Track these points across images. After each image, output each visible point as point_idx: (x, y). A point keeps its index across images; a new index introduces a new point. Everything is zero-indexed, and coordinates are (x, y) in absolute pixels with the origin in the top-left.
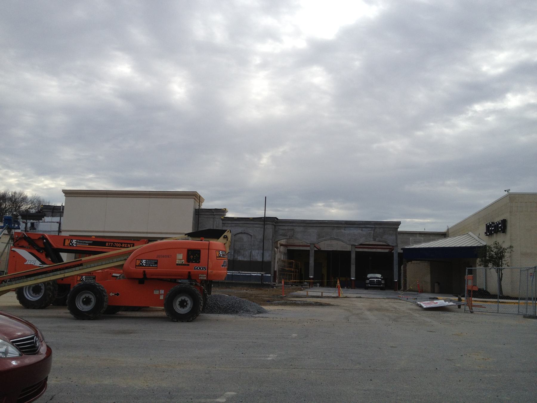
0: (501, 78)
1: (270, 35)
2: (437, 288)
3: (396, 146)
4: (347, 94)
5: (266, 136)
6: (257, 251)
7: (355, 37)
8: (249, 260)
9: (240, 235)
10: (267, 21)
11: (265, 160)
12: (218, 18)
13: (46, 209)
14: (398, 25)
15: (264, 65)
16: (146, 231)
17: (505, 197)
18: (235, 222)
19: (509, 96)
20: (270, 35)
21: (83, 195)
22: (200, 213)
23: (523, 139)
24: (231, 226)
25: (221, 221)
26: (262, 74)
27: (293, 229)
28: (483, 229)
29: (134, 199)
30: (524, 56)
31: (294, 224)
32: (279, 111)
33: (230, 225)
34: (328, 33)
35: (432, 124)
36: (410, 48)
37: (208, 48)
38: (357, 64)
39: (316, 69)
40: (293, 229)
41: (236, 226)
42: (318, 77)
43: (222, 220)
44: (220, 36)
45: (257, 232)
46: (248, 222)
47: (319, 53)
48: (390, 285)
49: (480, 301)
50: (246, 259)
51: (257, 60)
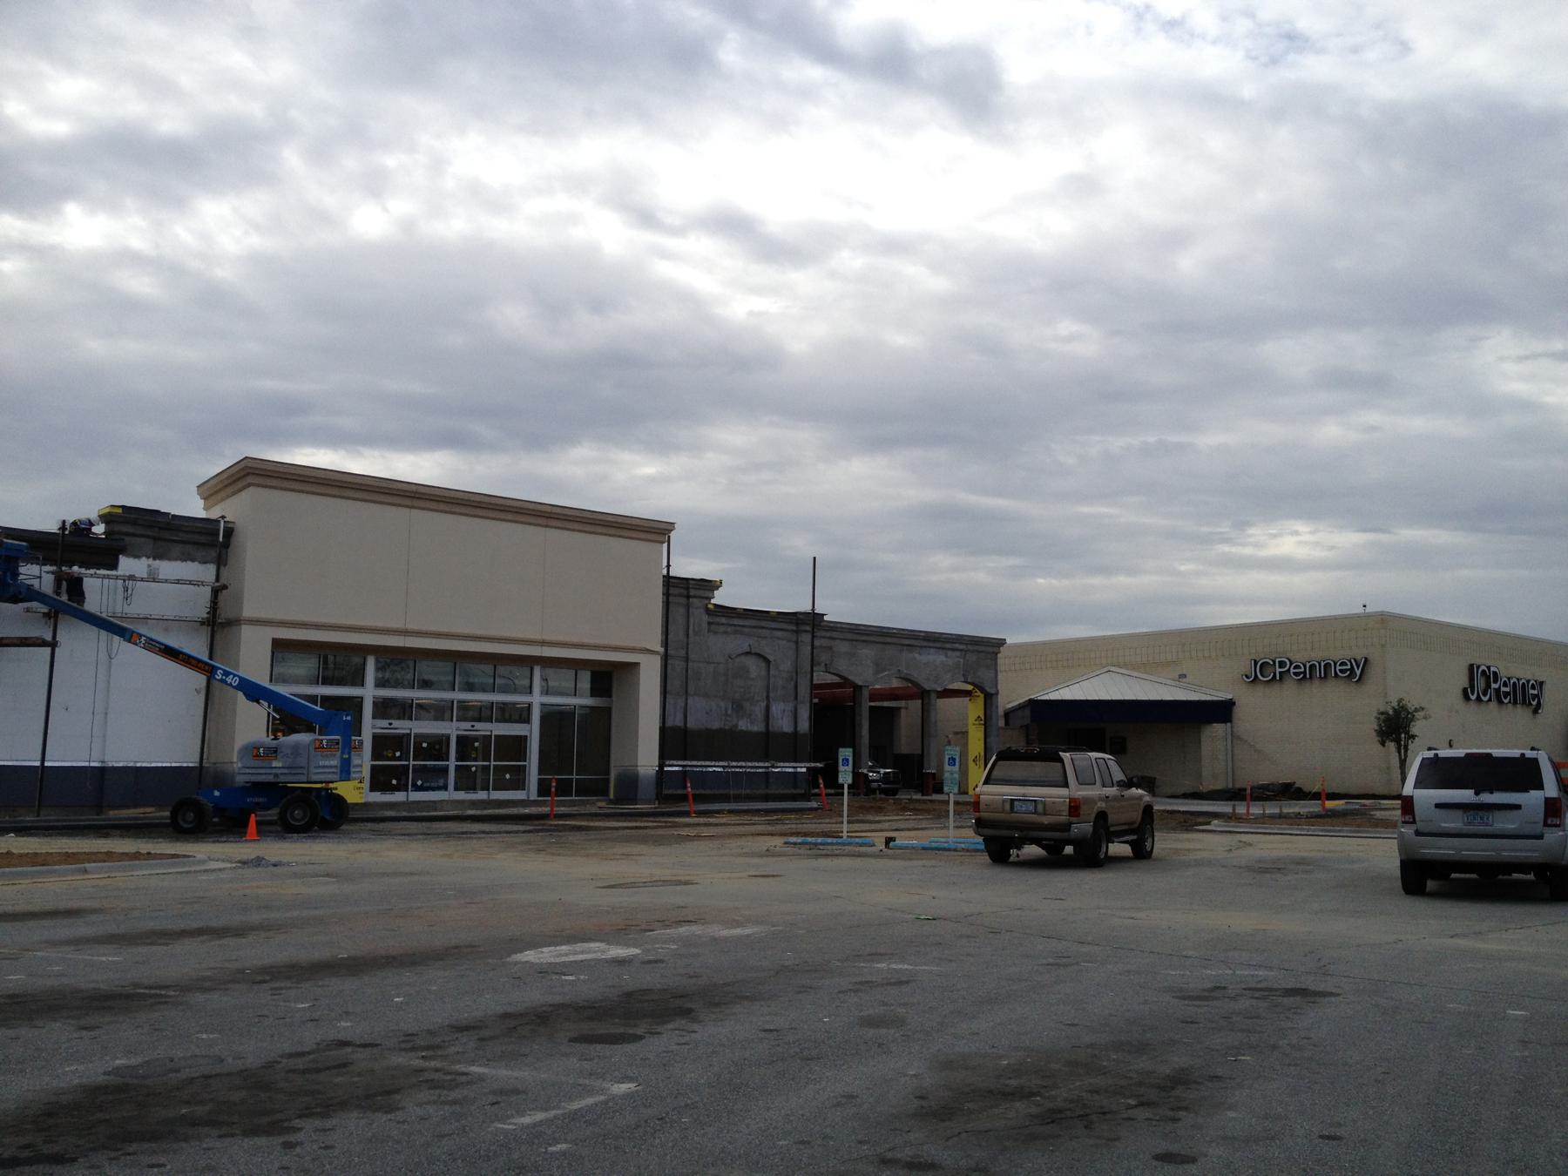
0: (56, 152)
2: (441, 782)
6: (781, 706)
8: (758, 727)
9: (743, 659)
13: (135, 523)
16: (538, 637)
17: (1358, 616)
18: (736, 622)
19: (72, 210)
21: (442, 507)
22: (692, 592)
23: (95, 347)
24: (726, 632)
25: (705, 618)
27: (830, 648)
28: (1244, 665)
29: (520, 527)
30: (131, 107)
31: (834, 634)
33: (722, 629)
40: (830, 648)
41: (735, 633)
43: (708, 611)
45: (779, 649)
46: (763, 624)
49: (731, 812)
50: (755, 729)
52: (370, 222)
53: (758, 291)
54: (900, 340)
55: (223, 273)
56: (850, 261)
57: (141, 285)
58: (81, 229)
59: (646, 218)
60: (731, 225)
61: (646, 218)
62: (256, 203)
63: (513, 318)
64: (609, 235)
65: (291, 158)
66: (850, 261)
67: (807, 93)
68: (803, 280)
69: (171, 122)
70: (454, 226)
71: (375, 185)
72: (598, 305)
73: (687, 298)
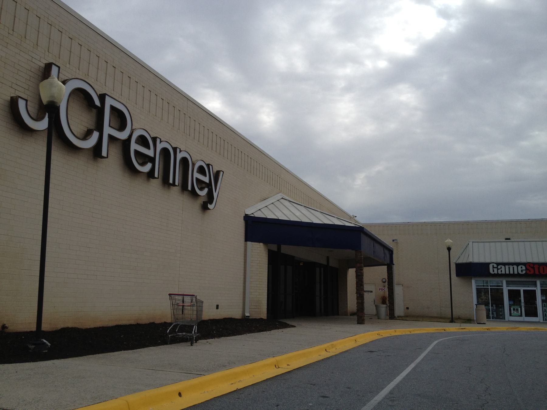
1: (350, 58)
3: (502, 158)
4: (439, 108)
5: (357, 156)
7: (435, 51)
10: (342, 47)
11: (360, 180)
12: (297, 48)
14: (484, 31)
15: (349, 89)
20: (350, 58)
26: (348, 97)
32: (369, 130)
34: (408, 51)
35: (537, 133)
36: (491, 56)
37: (291, 78)
38: (445, 78)
39: (402, 87)
42: (406, 96)
44: (300, 66)
47: (402, 71)
48: (357, 298)
51: (342, 84)
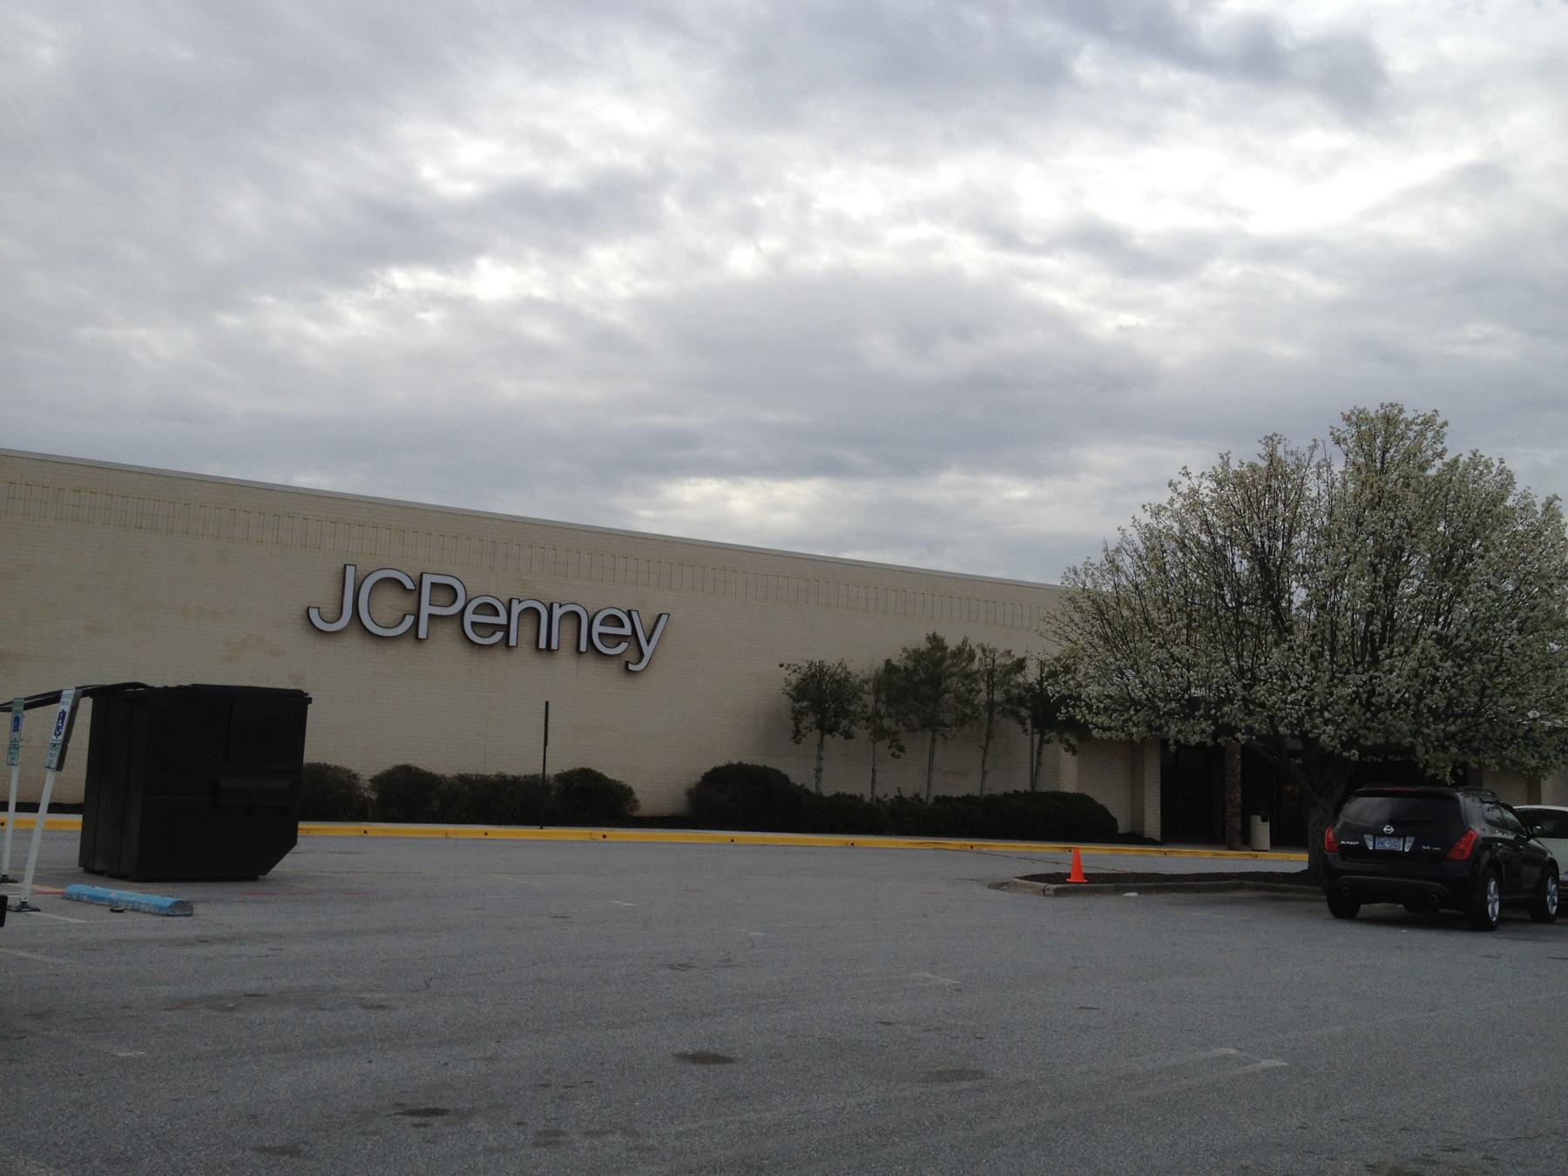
0: (469, 212)
52: (742, 262)
53: (1126, 306)
54: (1287, 350)
55: (615, 317)
56: (1226, 271)
57: (542, 331)
58: (494, 281)
59: (1006, 238)
60: (1098, 241)
61: (1006, 238)
62: (639, 249)
63: (882, 351)
64: (970, 256)
65: (670, 203)
66: (1226, 271)
67: (1172, 100)
68: (1173, 294)
69: (561, 176)
70: (822, 259)
71: (748, 225)
72: (963, 332)
73: (1052, 318)
